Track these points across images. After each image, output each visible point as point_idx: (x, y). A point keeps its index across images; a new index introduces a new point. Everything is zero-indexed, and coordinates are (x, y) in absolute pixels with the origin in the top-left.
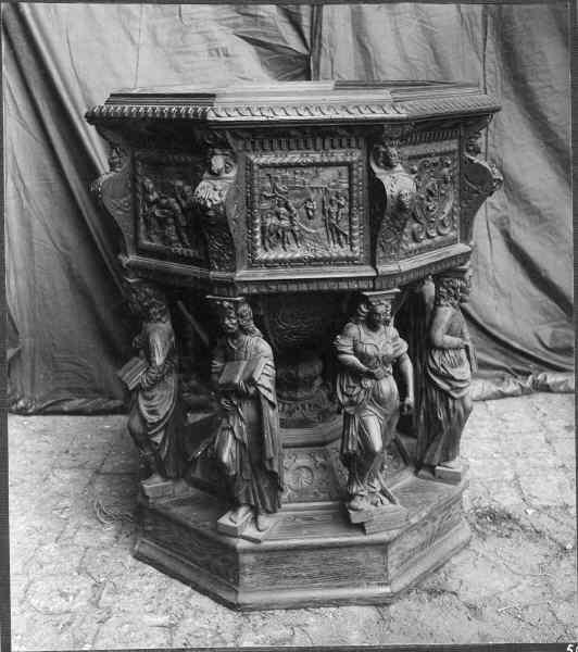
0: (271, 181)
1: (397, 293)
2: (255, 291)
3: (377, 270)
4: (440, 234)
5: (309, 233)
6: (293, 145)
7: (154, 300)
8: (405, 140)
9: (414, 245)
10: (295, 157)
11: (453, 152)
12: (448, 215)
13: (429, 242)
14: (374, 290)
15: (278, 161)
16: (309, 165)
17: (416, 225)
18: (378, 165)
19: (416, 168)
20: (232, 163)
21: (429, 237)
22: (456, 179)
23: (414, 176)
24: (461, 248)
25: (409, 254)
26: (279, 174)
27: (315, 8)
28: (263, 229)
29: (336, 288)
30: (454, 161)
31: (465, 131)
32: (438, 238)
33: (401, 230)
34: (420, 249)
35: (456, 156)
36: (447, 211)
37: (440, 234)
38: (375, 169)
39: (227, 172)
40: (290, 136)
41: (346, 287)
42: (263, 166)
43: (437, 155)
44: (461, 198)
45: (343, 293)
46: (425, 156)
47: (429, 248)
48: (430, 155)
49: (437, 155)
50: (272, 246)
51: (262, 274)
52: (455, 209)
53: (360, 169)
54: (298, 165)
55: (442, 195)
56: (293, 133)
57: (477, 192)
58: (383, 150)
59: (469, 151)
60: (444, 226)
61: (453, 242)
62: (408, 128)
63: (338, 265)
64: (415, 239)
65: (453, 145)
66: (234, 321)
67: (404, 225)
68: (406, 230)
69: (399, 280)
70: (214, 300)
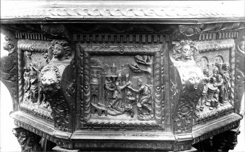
24: (234, 116)
38: (172, 60)
40: (111, 32)
42: (93, 54)
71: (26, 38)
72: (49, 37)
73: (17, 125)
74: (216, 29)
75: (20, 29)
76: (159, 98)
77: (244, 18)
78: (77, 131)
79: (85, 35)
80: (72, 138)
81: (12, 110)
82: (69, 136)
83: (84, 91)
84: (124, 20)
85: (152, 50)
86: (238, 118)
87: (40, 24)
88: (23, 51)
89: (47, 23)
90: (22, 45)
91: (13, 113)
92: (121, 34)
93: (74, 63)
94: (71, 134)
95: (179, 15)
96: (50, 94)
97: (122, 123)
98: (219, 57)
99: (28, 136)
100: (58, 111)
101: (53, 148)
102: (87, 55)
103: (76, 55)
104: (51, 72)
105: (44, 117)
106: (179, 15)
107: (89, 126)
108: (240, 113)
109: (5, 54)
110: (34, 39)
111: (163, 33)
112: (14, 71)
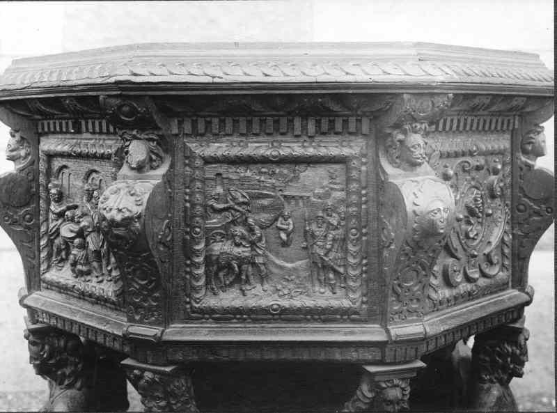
0: (222, 184)
1: (420, 369)
2: (196, 358)
3: (388, 331)
4: (484, 275)
5: (281, 268)
6: (256, 127)
7: (65, 355)
8: (436, 123)
9: (446, 293)
10: (258, 147)
11: (501, 153)
12: (497, 247)
13: (469, 287)
14: (381, 363)
15: (236, 151)
16: (283, 161)
17: (450, 261)
18: (392, 162)
19: (451, 172)
20: (162, 154)
21: (468, 279)
22: (509, 192)
23: (449, 183)
24: (511, 295)
25: (437, 306)
26: (232, 173)
27: (52, 238)
28: (208, 261)
29: (241, 358)
30: (504, 165)
31: (521, 122)
32: (482, 282)
33: (427, 269)
34: (456, 298)
35: (508, 159)
36: (495, 240)
37: (484, 275)
38: (389, 169)
39: (152, 168)
40: (252, 113)
41: (273, 357)
42: (208, 161)
43: (482, 153)
44: (513, 222)
45: (332, 366)
46: (464, 154)
47: (470, 296)
48: (471, 154)
49: (482, 153)
50: (225, 288)
51: (203, 333)
52: (506, 239)
53: (364, 168)
54: (264, 161)
55: (489, 215)
56: (257, 107)
57: (537, 213)
58: (401, 137)
59: (525, 152)
60: (491, 263)
61: (502, 287)
62: (441, 102)
63: (324, 321)
64: (448, 283)
65: (503, 143)
66: (163, 403)
67: (433, 262)
68: (435, 268)
69: (423, 349)
70: (133, 368)
71: (84, 128)
72: (202, 113)
73: (35, 322)
74: (474, 108)
75: (37, 111)
76: (354, 254)
77: (552, 83)
78: (173, 326)
79: (208, 119)
80: (166, 338)
81: (26, 292)
82: (159, 335)
83: (193, 238)
84: (309, 86)
85: (346, 151)
86: (519, 301)
87: (403, 93)
88: (51, 156)
89: (119, 92)
90: (49, 144)
91: (29, 297)
92: (262, 118)
93: (169, 179)
94: (161, 329)
95: (140, 75)
96: (124, 245)
97: (275, 307)
98: (415, 272)
99: (54, 348)
100: (137, 282)
101: (123, 360)
102: (199, 162)
103: (172, 166)
104: (126, 195)
105: (100, 301)
106: (140, 75)
107: (205, 314)
108: (526, 290)
109: (9, 168)
110: (64, 130)
111: (368, 114)
112: (16, 207)
